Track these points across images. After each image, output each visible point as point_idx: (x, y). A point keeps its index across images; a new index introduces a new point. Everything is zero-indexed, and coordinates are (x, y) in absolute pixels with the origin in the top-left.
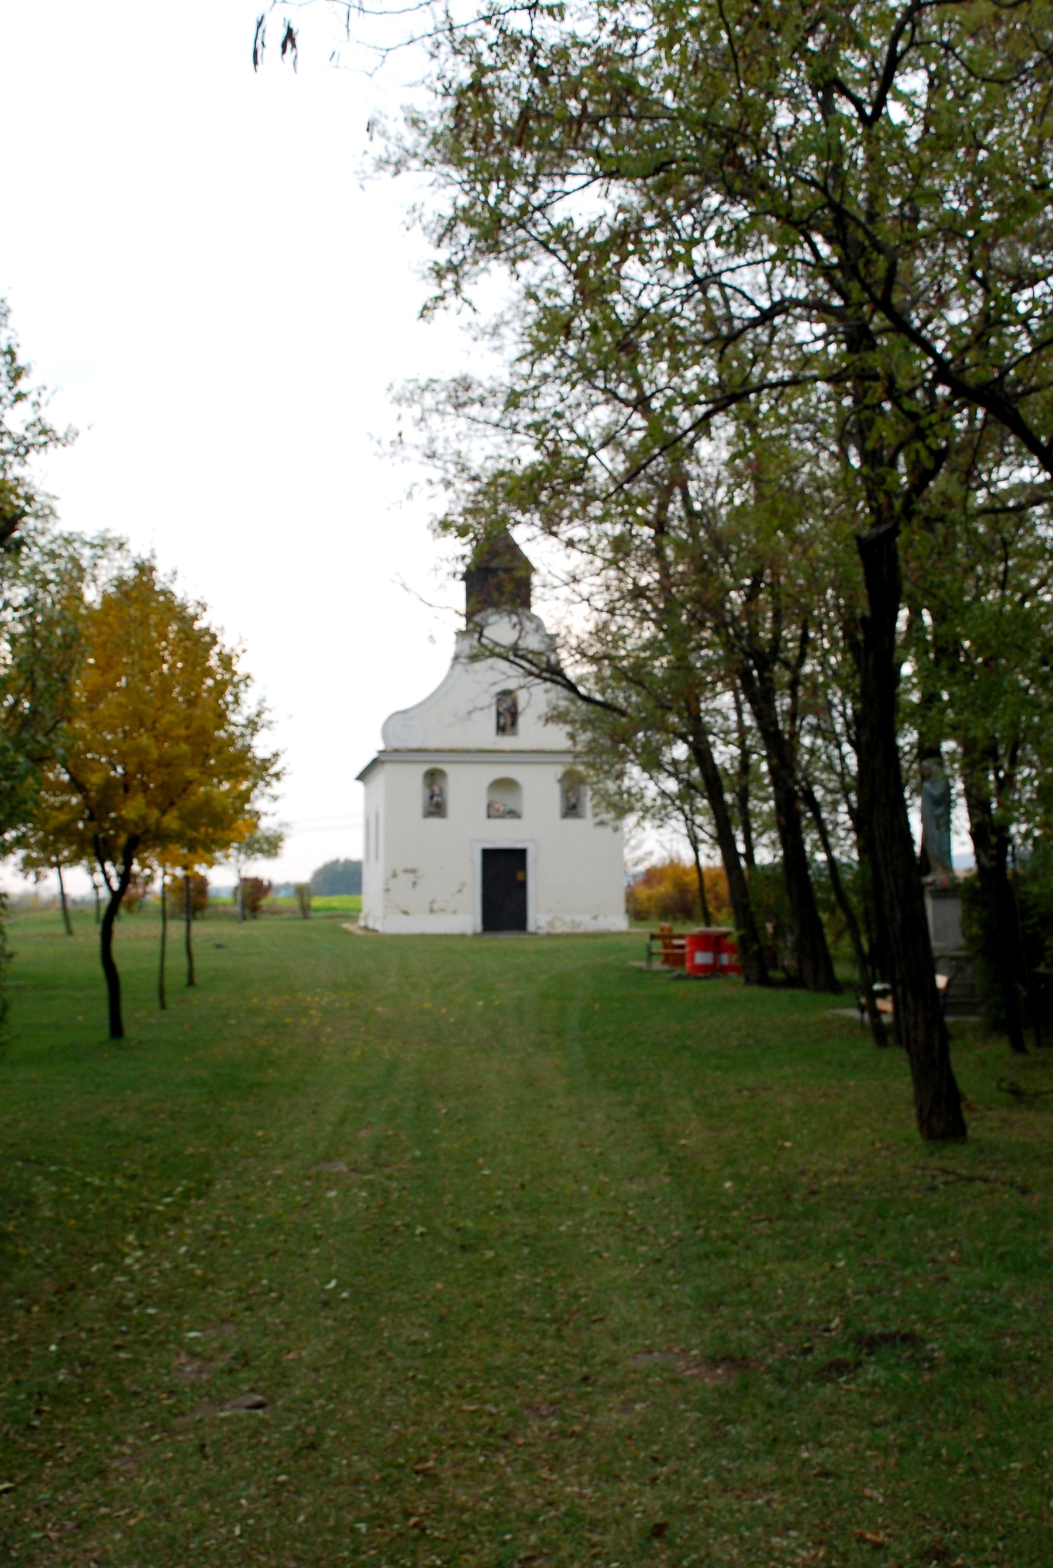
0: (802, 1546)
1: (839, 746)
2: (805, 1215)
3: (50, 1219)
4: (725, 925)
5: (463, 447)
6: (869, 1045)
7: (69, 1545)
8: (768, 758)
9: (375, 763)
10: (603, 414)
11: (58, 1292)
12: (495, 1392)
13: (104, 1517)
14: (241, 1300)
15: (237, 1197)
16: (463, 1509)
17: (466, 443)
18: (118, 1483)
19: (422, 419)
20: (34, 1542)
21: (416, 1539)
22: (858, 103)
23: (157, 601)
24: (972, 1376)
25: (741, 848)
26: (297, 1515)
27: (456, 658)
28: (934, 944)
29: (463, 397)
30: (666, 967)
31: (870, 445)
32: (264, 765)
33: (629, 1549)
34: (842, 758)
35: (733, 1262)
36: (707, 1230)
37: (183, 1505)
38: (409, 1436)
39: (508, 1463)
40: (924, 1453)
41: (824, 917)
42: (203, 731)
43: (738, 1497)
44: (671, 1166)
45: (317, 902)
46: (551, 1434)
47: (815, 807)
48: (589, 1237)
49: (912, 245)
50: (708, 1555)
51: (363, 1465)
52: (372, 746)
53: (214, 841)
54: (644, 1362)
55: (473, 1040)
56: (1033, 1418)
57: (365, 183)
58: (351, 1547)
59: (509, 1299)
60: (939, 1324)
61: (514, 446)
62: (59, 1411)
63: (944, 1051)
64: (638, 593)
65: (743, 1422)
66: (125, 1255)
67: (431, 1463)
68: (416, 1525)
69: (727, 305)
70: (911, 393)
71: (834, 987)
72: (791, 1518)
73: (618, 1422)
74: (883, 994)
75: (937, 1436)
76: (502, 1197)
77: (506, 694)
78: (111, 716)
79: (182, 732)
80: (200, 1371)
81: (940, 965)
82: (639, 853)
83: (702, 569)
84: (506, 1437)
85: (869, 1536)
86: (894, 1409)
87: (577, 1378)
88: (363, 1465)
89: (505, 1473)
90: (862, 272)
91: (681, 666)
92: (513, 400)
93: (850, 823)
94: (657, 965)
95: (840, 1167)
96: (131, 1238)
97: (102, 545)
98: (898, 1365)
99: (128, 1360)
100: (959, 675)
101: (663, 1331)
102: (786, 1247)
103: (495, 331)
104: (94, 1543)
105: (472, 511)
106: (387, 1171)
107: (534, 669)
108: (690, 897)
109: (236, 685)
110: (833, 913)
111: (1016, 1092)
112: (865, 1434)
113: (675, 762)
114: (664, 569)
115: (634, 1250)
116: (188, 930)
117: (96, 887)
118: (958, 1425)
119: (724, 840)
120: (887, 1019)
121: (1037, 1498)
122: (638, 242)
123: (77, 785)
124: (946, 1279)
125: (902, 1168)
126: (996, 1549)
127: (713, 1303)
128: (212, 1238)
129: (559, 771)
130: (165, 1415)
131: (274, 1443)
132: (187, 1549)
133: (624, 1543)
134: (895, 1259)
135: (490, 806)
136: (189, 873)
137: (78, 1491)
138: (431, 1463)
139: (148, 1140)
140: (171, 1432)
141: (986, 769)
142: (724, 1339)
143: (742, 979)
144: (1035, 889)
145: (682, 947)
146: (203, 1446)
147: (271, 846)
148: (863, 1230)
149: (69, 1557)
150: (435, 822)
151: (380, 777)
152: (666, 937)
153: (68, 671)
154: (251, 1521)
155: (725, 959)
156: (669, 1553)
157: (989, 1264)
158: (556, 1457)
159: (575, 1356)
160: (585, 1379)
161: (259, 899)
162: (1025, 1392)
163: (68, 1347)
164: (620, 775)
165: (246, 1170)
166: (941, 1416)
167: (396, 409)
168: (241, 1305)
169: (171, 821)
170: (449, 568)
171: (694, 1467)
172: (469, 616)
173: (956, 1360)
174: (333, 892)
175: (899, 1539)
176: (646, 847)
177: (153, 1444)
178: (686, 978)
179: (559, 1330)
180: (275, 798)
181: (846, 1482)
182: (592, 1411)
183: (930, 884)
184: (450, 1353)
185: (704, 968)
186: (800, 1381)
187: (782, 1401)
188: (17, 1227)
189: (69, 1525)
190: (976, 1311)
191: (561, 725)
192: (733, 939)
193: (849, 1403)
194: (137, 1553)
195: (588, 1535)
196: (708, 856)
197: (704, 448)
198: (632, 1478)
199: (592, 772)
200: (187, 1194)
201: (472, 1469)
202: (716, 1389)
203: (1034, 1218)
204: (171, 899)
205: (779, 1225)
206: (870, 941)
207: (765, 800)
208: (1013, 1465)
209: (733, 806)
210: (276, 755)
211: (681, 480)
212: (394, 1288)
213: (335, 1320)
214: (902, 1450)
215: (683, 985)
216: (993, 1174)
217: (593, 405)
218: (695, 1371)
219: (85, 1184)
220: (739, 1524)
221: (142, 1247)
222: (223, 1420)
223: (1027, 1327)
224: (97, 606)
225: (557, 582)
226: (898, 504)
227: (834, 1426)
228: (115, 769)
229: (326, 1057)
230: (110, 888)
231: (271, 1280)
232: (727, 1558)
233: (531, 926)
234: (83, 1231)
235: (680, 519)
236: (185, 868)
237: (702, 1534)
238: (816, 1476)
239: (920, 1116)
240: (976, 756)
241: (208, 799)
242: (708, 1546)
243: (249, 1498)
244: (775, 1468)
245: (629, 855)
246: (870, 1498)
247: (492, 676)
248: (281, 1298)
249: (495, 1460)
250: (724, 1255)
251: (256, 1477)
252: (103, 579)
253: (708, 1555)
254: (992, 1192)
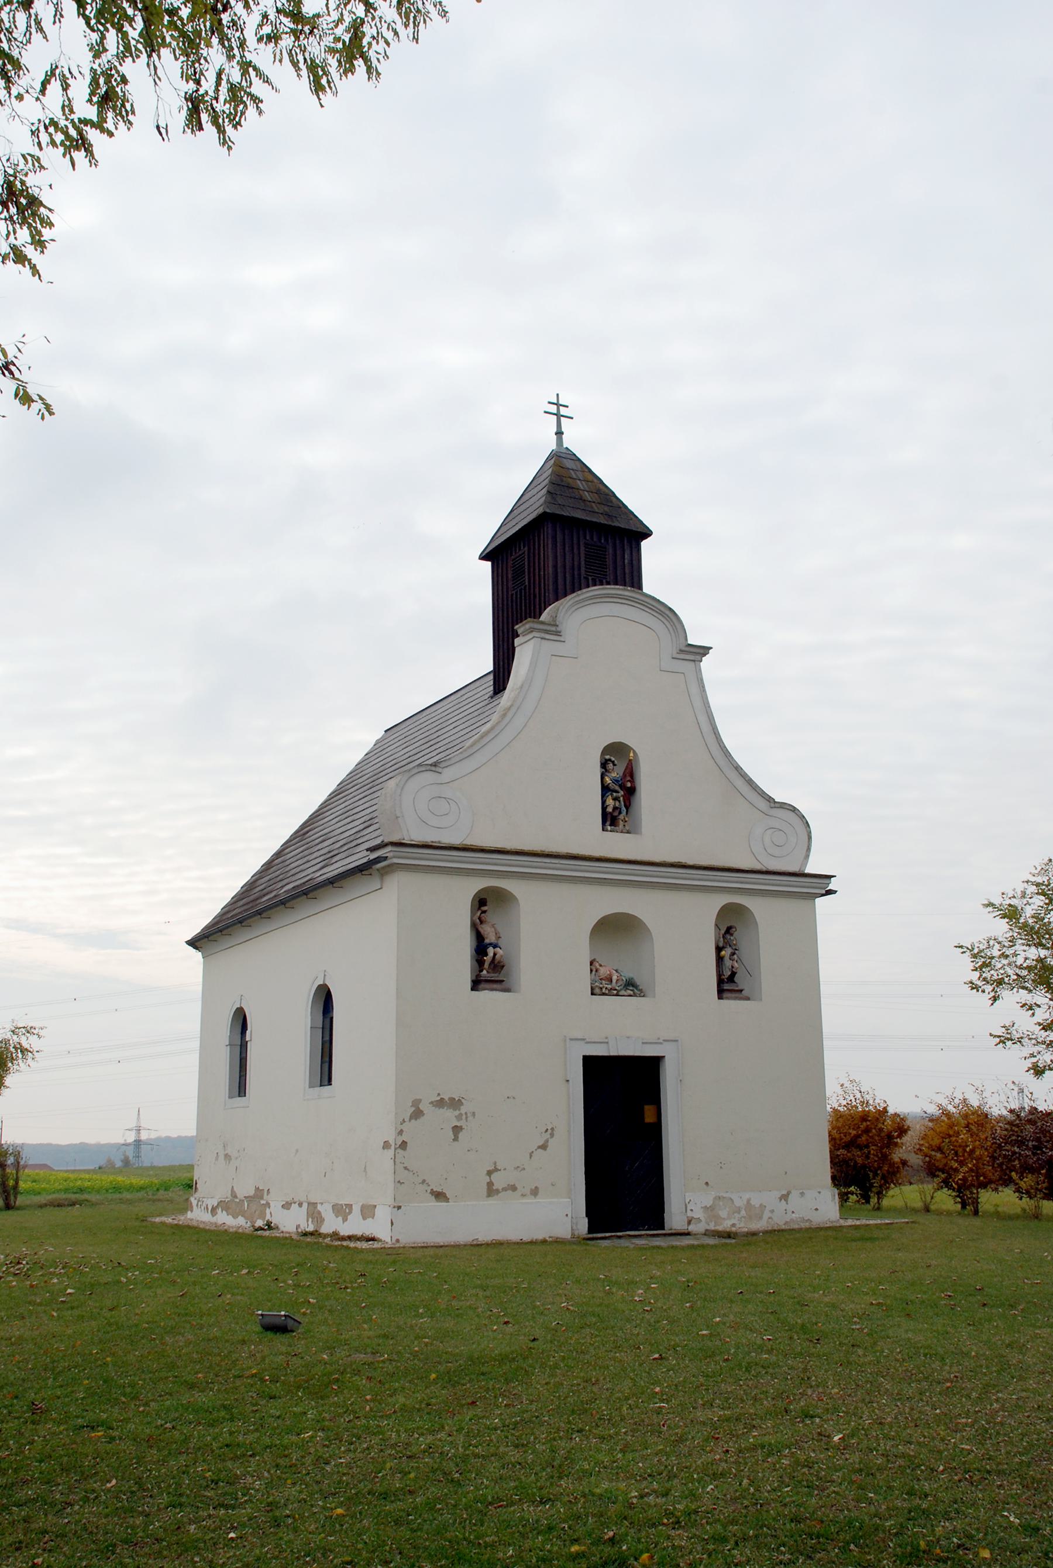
135: (592, 989)
150: (487, 996)
233: (675, 1217)
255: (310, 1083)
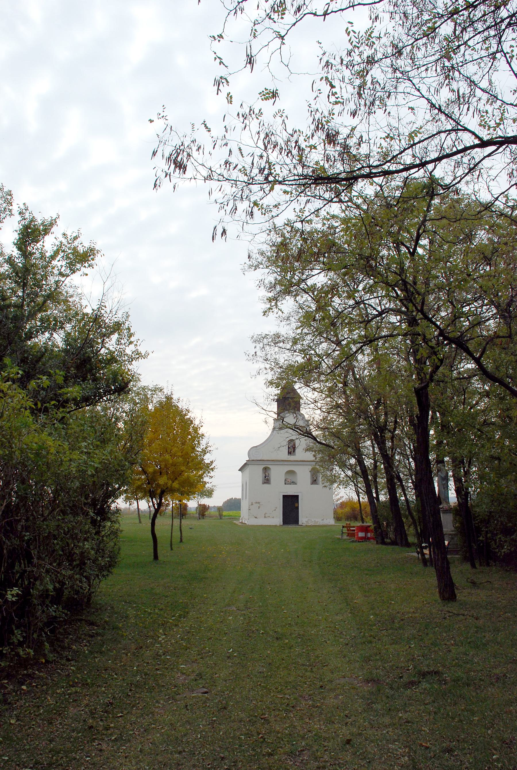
0: (400, 748)
1: (408, 460)
2: (400, 628)
3: (133, 623)
4: (369, 522)
5: (277, 357)
6: (421, 566)
7: (142, 737)
8: (384, 463)
9: (245, 464)
10: (324, 345)
11: (136, 649)
12: (289, 691)
13: (153, 728)
14: (199, 655)
15: (197, 618)
16: (278, 732)
17: (278, 355)
18: (157, 717)
19: (263, 348)
20: (131, 735)
21: (262, 742)
22: (408, 248)
23: (173, 409)
24: (460, 686)
25: (375, 495)
26: (220, 732)
27: (274, 429)
28: (444, 530)
29: (277, 340)
30: (348, 538)
31: (418, 357)
32: (208, 466)
33: (338, 748)
34: (409, 463)
35: (374, 645)
36: (364, 633)
37: (180, 726)
38: (259, 706)
39: (294, 716)
40: (443, 714)
41: (404, 520)
42: (187, 454)
43: (377, 730)
44: (351, 610)
45: (225, 513)
46: (309, 706)
47: (400, 480)
48: (322, 635)
49: (428, 293)
50: (366, 751)
51: (243, 715)
52: (245, 458)
53: (190, 492)
54: (342, 681)
55: (280, 563)
56: (481, 701)
57: (245, 273)
58: (239, 744)
59: (294, 658)
60: (448, 668)
61: (295, 356)
62: (137, 690)
63: (448, 568)
64: (338, 406)
65: (378, 703)
66: (159, 637)
67: (267, 716)
68: (262, 737)
69: (366, 310)
70: (430, 340)
71: (408, 545)
72: (396, 738)
73: (333, 702)
74: (426, 548)
75: (448, 708)
76: (291, 620)
77: (292, 440)
78: (156, 449)
79: (180, 454)
80: (185, 679)
81: (445, 537)
82: (338, 497)
83: (359, 397)
84: (293, 707)
85: (424, 744)
86: (432, 698)
87: (318, 686)
88: (242, 715)
89: (293, 720)
90: (413, 301)
91: (353, 432)
92: (295, 341)
93: (412, 487)
94: (345, 537)
95: (412, 610)
96: (161, 631)
97: (157, 390)
98: (433, 682)
99: (160, 674)
100: (450, 435)
101: (349, 670)
102: (392, 639)
103: (288, 319)
104: (150, 737)
105: (281, 379)
106: (250, 610)
107: (301, 432)
108: (356, 512)
109: (199, 438)
110: (407, 519)
111: (474, 583)
112: (422, 708)
113: (351, 465)
114: (347, 398)
115: (338, 640)
116: (181, 522)
117: (149, 507)
118: (455, 704)
119: (369, 492)
120: (427, 557)
121: (483, 730)
122: (338, 291)
123: (144, 472)
124: (450, 651)
125: (434, 611)
126: (469, 749)
127: (367, 660)
128: (189, 632)
129: (310, 468)
130: (173, 694)
131: (211, 706)
132: (182, 741)
133: (336, 746)
134: (432, 644)
136: (181, 503)
137: (144, 719)
138: (267, 716)
139: (167, 597)
140: (176, 700)
141: (460, 468)
142: (371, 673)
143: (375, 542)
144: (478, 510)
145: (354, 530)
146: (187, 706)
147: (209, 493)
148: (420, 634)
149: (142, 741)
150: (266, 485)
151: (247, 470)
152: (348, 527)
153: (143, 433)
154: (204, 733)
155: (369, 535)
156: (352, 750)
157: (465, 645)
158: (311, 715)
159: (317, 678)
160: (321, 687)
161: (205, 512)
162: (478, 691)
163: (140, 668)
164: (332, 470)
165: (200, 608)
166: (449, 701)
167: (254, 344)
168: (199, 657)
169: (176, 485)
170: (272, 398)
171: (361, 719)
172: (278, 414)
173: (454, 681)
174: (230, 510)
175: (435, 745)
176: (341, 495)
177: (169, 704)
178: (356, 542)
179: (312, 669)
180: (211, 477)
181: (416, 725)
182: (324, 698)
183: (441, 508)
184: (273, 676)
185: (362, 538)
186: (398, 688)
187: (392, 695)
188: (122, 625)
189: (142, 730)
190: (461, 663)
191: (311, 452)
192: (372, 528)
193: (416, 696)
194: (165, 742)
195: (323, 743)
196: (363, 498)
197: (360, 357)
198: (338, 723)
199: (322, 469)
200: (180, 616)
201: (281, 718)
202: (368, 691)
203: (481, 628)
204: (175, 512)
205: (390, 631)
206: (420, 529)
207: (382, 478)
208: (475, 718)
209: (372, 480)
210: (212, 462)
211: (351, 368)
212: (253, 652)
213: (232, 663)
214: (435, 713)
215: (354, 544)
216: (466, 613)
217: (321, 343)
218: (361, 684)
219: (145, 611)
220: (377, 740)
221: (165, 634)
222: (193, 697)
223: (479, 668)
224: (153, 411)
225: (309, 403)
226: (428, 377)
227: (411, 705)
228: (157, 467)
229: (228, 569)
230: (154, 507)
231: (209, 648)
232: (373, 752)
233: (300, 523)
234: (145, 628)
235: (352, 381)
236: (180, 501)
237: (364, 743)
238: (404, 723)
239: (440, 592)
240: (457, 463)
241: (188, 477)
242: (366, 747)
243: (203, 725)
244: (390, 720)
245: (335, 498)
246: (424, 731)
247: (287, 435)
248: (213, 655)
249: (289, 715)
250: (371, 642)
251: (205, 718)
252: (155, 402)
253: (366, 751)
254: (465, 619)
255: (298, 498)
